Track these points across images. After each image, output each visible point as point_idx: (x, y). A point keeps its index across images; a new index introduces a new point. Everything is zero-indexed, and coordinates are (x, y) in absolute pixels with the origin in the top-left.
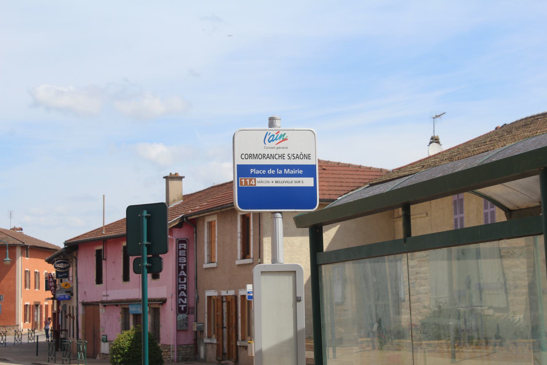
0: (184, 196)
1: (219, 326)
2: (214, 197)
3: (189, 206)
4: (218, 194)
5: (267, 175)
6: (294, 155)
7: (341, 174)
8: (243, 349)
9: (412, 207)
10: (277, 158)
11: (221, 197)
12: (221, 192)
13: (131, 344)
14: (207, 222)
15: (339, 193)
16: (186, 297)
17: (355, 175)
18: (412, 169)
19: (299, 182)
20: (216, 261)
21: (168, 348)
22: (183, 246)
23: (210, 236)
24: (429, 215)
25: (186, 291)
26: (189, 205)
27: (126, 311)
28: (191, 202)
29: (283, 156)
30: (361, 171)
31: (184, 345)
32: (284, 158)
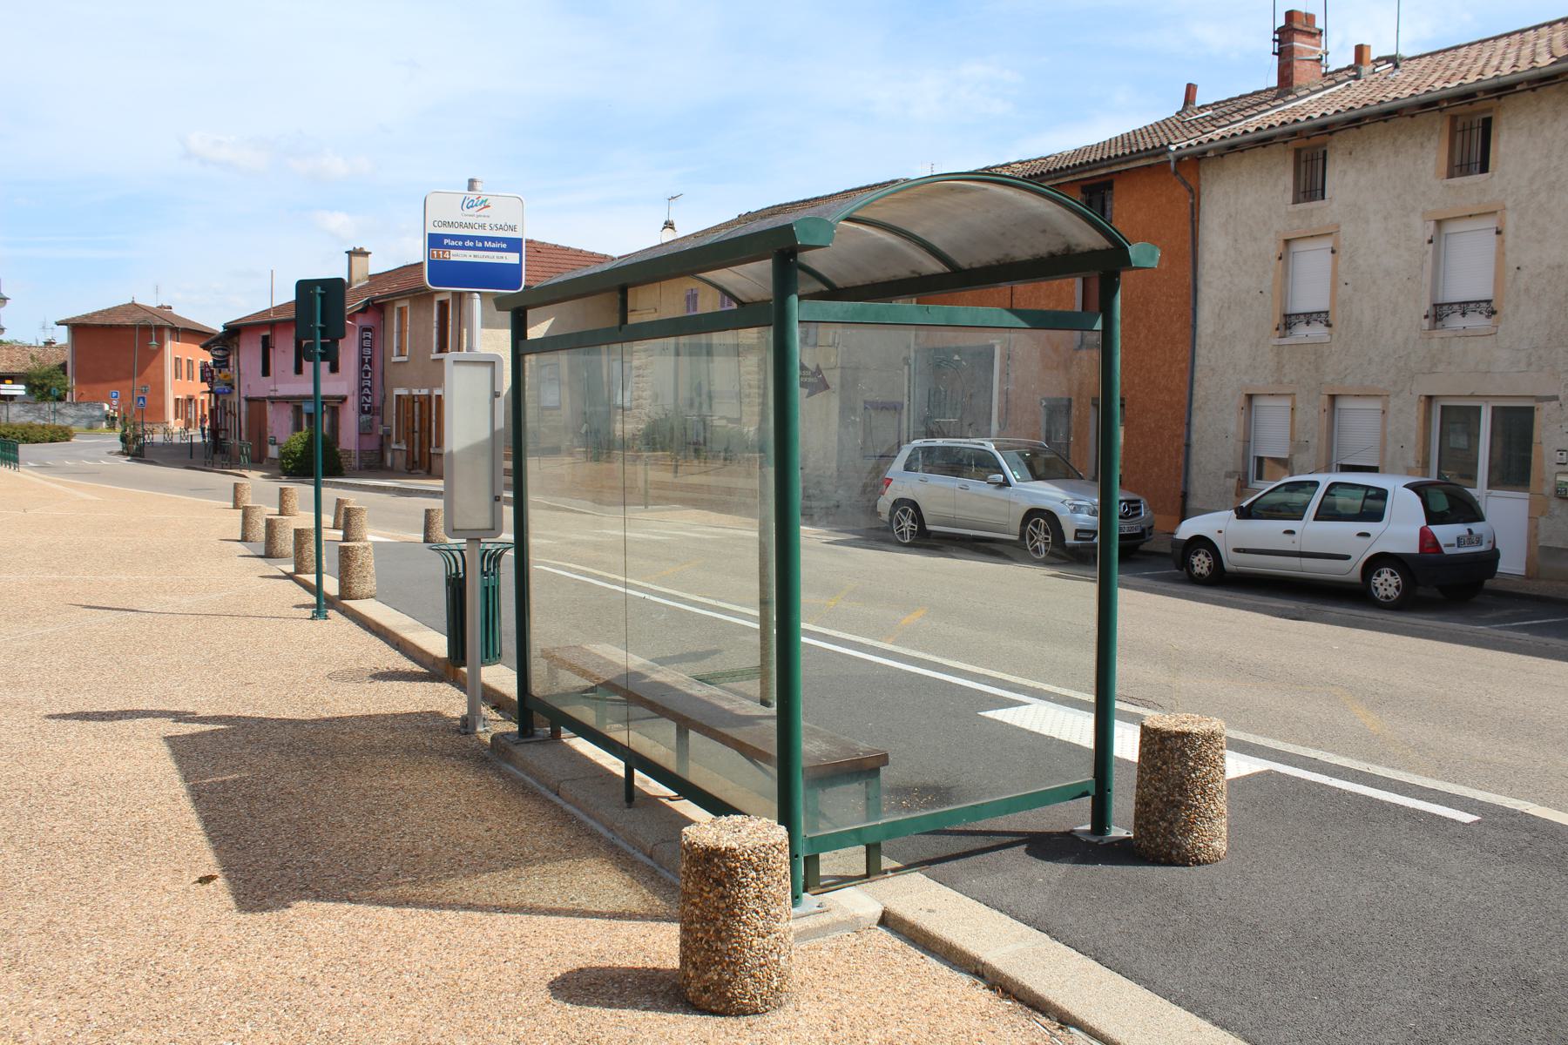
5: (464, 248)
19: (502, 257)
25: (370, 389)
27: (298, 410)
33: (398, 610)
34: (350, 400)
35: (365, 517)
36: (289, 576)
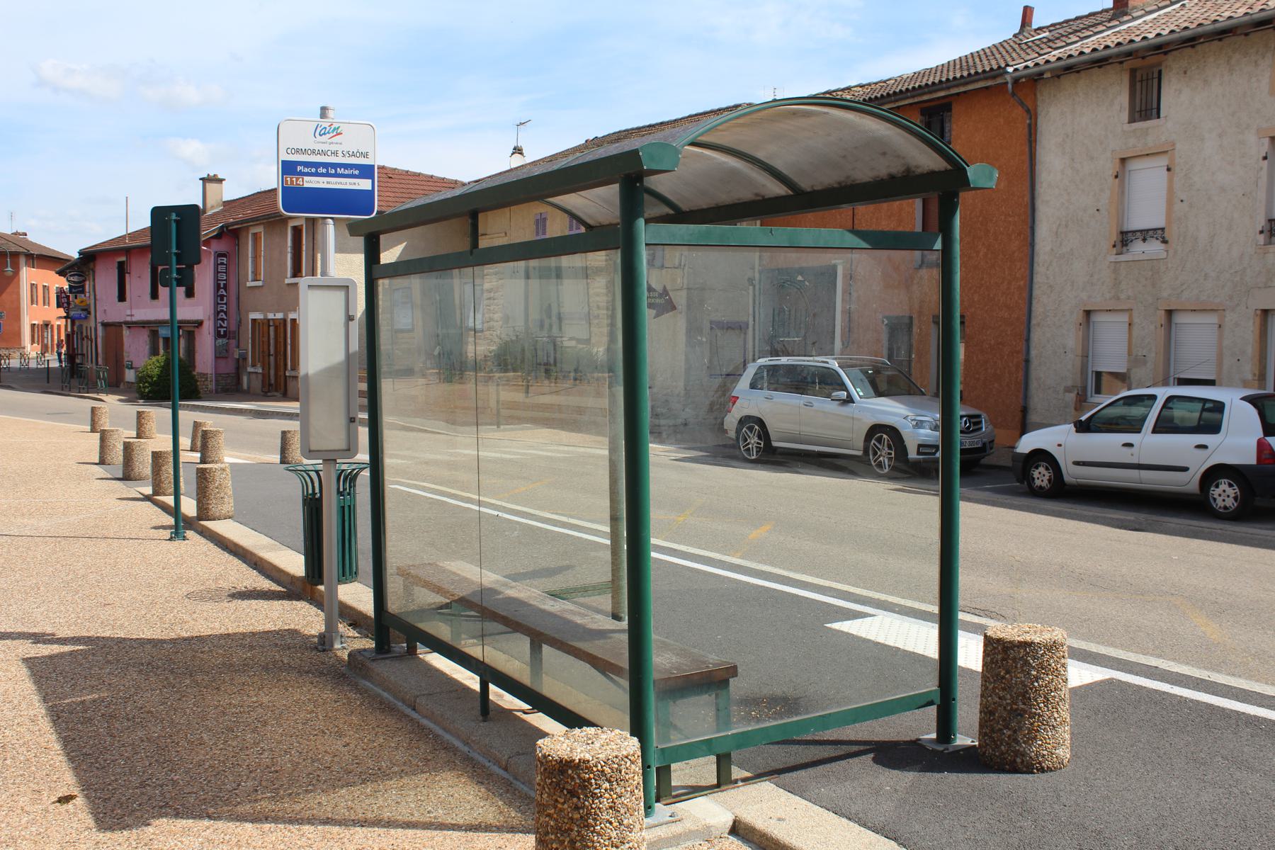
0: (224, 202)
24: (508, 234)
25: (226, 313)
27: (154, 334)
33: (256, 531)
34: (206, 324)
35: (222, 439)
36: (147, 498)
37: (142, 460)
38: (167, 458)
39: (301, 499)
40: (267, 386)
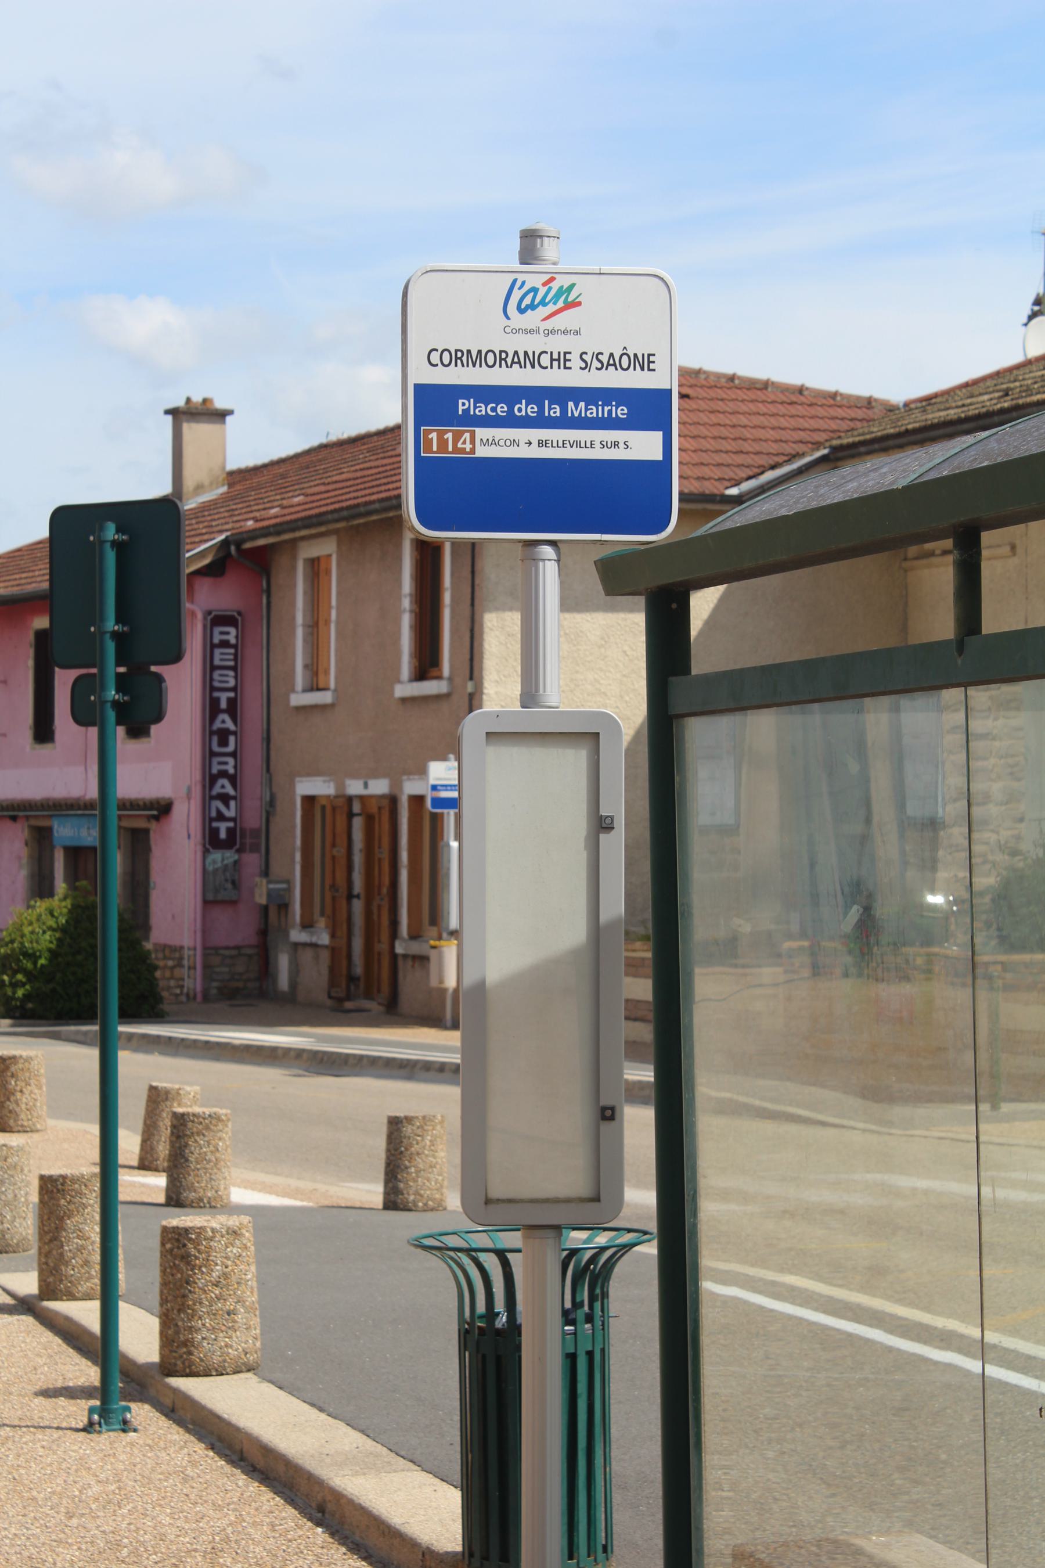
0: (231, 474)
1: (337, 891)
2: (326, 478)
3: (248, 506)
4: (341, 469)
5: (511, 421)
6: (600, 357)
7: (738, 413)
8: (413, 966)
9: (987, 537)
10: (544, 365)
11: (350, 480)
12: (350, 464)
13: (59, 940)
14: (306, 560)
15: (732, 475)
16: (234, 798)
17: (783, 416)
18: (969, 401)
19: (616, 444)
20: (332, 685)
21: (177, 955)
22: (228, 633)
23: (313, 606)
24: (1019, 550)
25: (233, 780)
26: (246, 502)
27: (41, 838)
28: (253, 493)
29: (565, 360)
30: (802, 404)
31: (227, 948)
32: (568, 364)
33: (321, 1410)
34: (179, 812)
35: (225, 1138)
36: (24, 1306)
37: (10, 1196)
38: (81, 1194)
39: (456, 1327)
40: (344, 985)
